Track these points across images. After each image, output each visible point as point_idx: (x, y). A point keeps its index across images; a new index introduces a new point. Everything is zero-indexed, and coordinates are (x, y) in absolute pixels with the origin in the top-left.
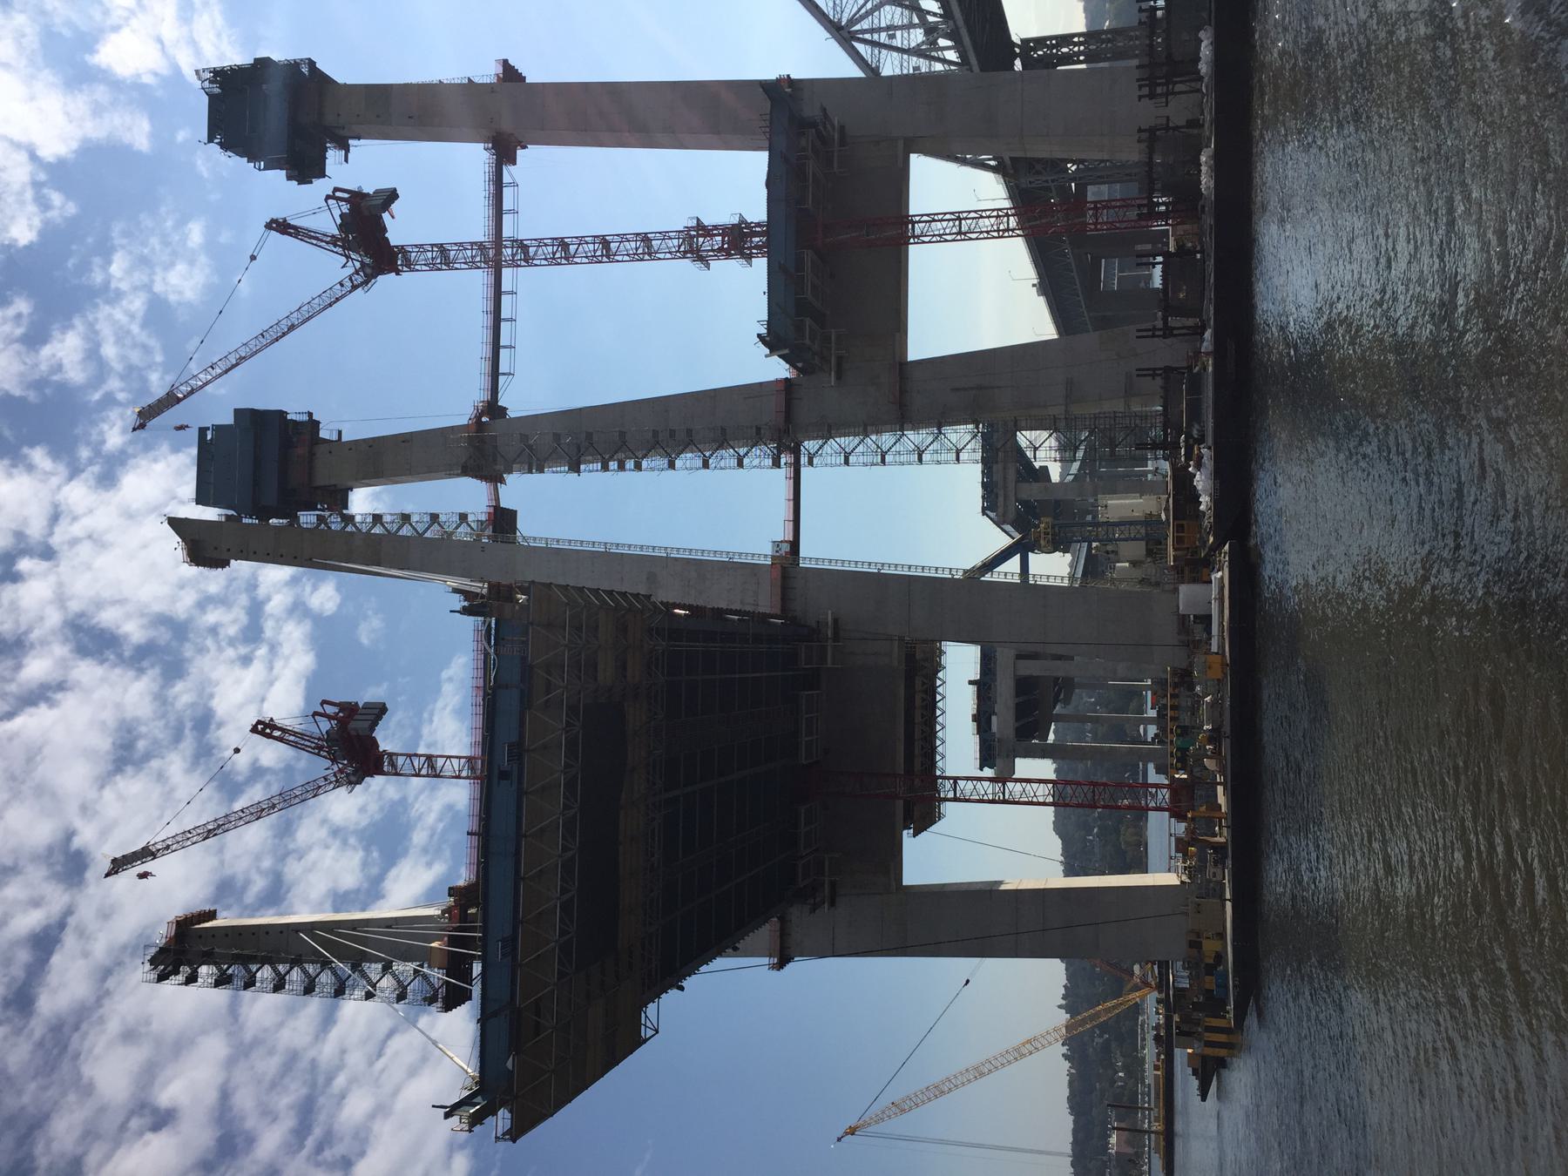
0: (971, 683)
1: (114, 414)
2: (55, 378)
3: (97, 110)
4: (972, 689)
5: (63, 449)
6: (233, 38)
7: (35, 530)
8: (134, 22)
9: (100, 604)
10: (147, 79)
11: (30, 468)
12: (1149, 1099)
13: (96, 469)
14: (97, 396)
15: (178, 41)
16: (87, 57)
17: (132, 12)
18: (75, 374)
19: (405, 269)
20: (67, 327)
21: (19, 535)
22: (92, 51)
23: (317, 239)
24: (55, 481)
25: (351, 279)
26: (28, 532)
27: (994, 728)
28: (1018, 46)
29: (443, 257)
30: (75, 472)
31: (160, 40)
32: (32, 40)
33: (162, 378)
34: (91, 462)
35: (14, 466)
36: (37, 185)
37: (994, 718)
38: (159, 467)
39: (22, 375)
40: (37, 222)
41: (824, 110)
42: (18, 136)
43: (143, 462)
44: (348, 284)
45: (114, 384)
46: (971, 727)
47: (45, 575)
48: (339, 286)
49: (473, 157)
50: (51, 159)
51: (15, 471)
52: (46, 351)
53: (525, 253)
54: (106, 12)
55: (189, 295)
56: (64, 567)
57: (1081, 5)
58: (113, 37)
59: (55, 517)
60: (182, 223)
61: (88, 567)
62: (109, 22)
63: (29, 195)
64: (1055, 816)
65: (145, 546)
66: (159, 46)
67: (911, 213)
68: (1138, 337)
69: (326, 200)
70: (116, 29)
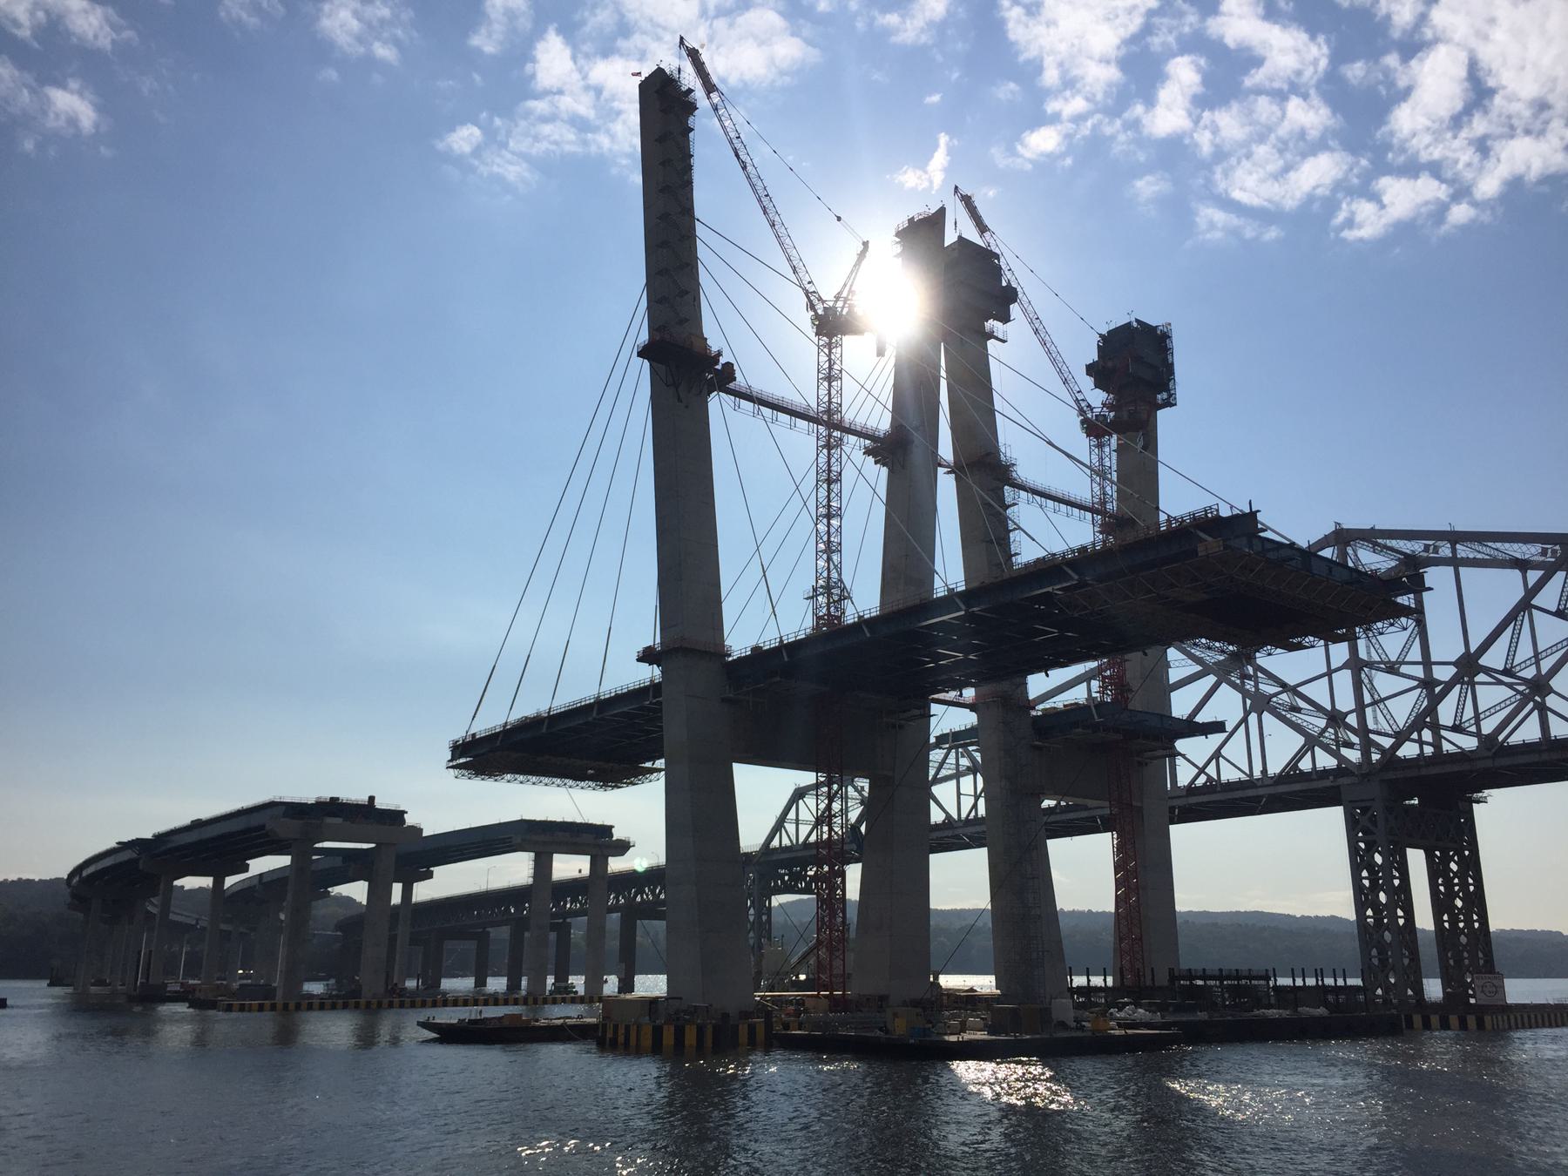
0: (372, 799)
4: (362, 798)
6: (552, 155)
8: (576, 76)
10: (529, 67)
12: (494, 1000)
15: (557, 107)
16: (555, 25)
22: (559, 32)
27: (329, 820)
31: (560, 92)
37: (339, 820)
46: (326, 794)
54: (587, 56)
55: (326, 23)
57: (1566, 933)
58: (568, 52)
60: (397, 43)
64: (1097, 913)
66: (555, 90)
68: (1316, 970)
70: (574, 58)
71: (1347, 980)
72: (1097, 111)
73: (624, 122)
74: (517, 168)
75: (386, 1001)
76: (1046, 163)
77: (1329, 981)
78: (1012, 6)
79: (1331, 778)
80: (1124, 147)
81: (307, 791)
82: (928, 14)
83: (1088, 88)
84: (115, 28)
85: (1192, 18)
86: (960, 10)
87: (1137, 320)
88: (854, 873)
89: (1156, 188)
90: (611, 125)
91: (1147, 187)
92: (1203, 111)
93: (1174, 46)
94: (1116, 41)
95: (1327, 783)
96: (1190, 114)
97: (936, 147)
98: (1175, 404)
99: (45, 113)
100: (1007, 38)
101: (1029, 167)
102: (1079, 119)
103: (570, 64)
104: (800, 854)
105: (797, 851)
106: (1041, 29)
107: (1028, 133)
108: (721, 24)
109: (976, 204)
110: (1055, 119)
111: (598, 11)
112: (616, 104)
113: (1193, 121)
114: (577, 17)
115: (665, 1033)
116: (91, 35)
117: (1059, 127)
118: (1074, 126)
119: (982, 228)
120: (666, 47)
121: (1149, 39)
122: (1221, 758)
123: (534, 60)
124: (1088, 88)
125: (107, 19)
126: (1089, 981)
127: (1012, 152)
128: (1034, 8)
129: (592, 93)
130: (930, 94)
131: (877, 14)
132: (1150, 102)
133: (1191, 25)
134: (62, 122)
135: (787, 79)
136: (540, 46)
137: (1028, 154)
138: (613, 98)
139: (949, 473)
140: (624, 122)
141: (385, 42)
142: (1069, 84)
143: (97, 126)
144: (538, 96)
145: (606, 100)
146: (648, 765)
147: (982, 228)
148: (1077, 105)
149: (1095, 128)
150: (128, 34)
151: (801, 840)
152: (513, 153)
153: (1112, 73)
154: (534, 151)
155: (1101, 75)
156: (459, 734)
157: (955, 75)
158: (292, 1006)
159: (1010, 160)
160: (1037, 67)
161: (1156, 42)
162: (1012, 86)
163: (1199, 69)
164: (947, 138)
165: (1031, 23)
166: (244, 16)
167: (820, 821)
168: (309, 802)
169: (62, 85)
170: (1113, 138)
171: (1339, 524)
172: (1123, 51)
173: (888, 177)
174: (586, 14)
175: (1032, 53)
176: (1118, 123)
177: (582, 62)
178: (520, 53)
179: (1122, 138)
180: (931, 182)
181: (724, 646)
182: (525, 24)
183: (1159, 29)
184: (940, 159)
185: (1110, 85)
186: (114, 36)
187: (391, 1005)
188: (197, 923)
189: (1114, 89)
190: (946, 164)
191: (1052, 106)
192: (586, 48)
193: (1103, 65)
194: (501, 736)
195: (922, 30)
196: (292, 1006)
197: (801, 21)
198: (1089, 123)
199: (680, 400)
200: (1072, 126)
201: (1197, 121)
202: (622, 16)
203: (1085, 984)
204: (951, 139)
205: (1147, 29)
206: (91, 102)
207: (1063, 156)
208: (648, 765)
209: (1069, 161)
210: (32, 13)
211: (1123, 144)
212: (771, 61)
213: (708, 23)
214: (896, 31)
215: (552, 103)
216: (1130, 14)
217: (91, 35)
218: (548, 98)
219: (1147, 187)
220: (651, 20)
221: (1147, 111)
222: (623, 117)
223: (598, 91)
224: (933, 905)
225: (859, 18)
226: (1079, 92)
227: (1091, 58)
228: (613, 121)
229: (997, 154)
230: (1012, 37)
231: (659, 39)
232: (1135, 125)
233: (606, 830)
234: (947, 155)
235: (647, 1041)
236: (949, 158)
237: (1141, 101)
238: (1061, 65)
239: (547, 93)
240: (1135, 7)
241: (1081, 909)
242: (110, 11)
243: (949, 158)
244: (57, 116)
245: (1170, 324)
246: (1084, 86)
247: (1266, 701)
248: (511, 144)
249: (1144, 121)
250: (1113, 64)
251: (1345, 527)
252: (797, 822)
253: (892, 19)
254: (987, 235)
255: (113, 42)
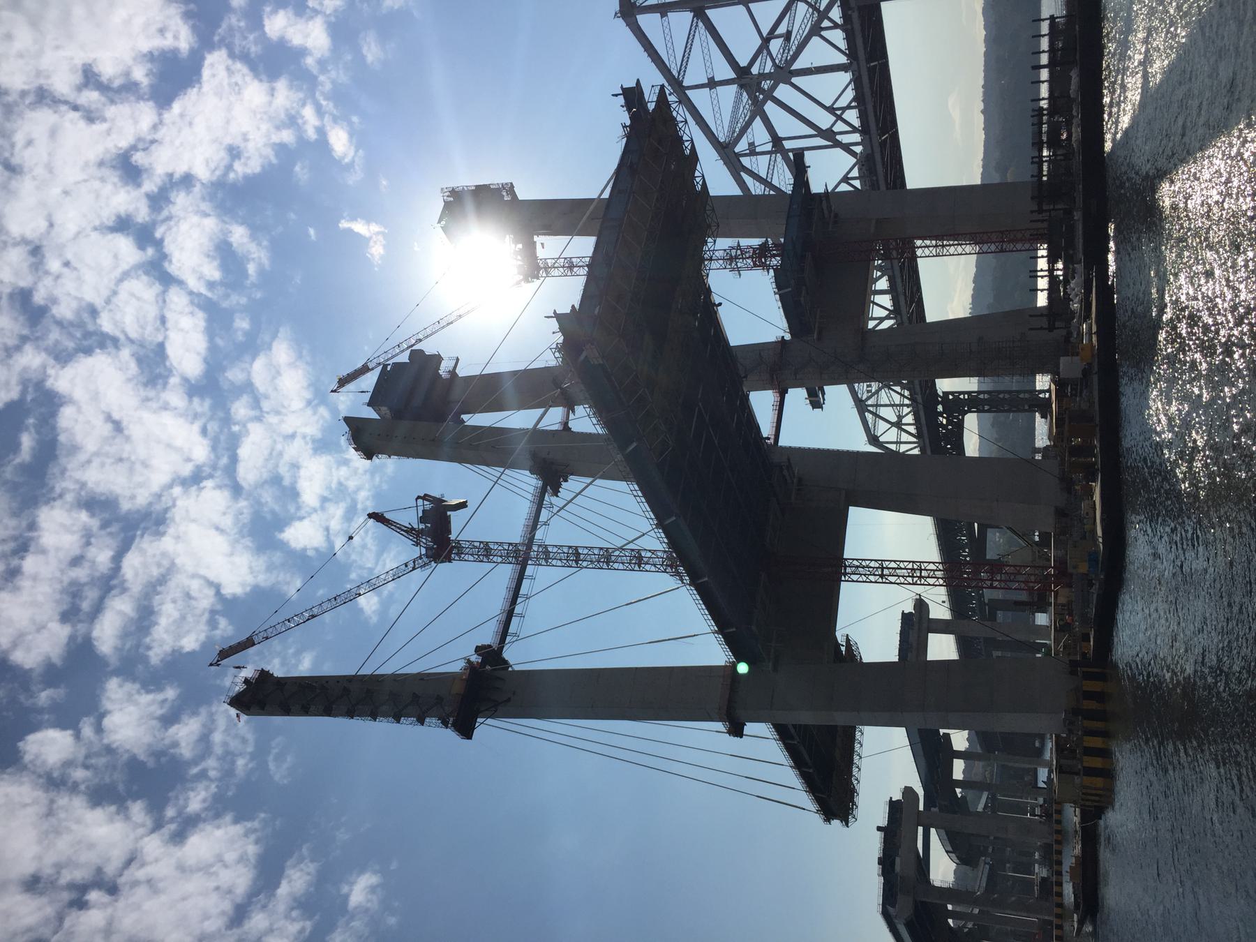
0: (879, 829)
1: (201, 786)
2: (172, 751)
3: (270, 568)
5: (156, 808)
7: (110, 870)
8: (314, 517)
9: (200, 88)
10: (310, 553)
11: (127, 818)
13: (173, 827)
14: (195, 771)
15: (339, 532)
16: (276, 533)
17: (315, 510)
18: (186, 752)
19: (457, 558)
20: (195, 713)
21: (99, 870)
22: (282, 531)
23: (399, 528)
24: (141, 831)
25: (414, 562)
26: (105, 870)
27: (898, 868)
28: (940, 397)
29: (485, 552)
30: (158, 826)
31: (327, 529)
32: (246, 518)
33: (246, 765)
34: (172, 820)
35: (118, 813)
36: (213, 612)
37: (898, 860)
38: (219, 833)
39: (149, 745)
40: (202, 637)
41: (789, 460)
42: (212, 576)
43: (209, 828)
44: (411, 565)
45: (211, 763)
46: (875, 869)
47: (104, 906)
48: (404, 566)
49: (527, 481)
50: (228, 597)
51: (118, 817)
52: (173, 730)
53: (546, 556)
54: (299, 508)
56: (121, 904)
58: (297, 524)
59: (129, 862)
60: (299, 653)
61: (138, 907)
62: (298, 514)
63: (206, 616)
65: (184, 899)
66: (326, 533)
67: (845, 557)
68: (1030, 277)
69: (416, 500)
70: (301, 519)
71: (1043, 33)
72: (313, 97)
73: (347, 479)
74: (388, 561)
75: (1056, 827)
76: (358, 138)
77: (1044, 59)
78: (234, 170)
79: (850, 12)
80: (341, 72)
81: (873, 884)
82: (245, 240)
83: (295, 105)
84: (301, 860)
85: (233, 20)
86: (240, 213)
87: (439, 222)
88: (945, 385)
89: (373, 45)
90: (350, 490)
91: (372, 51)
92: (308, 7)
93: (256, 34)
94: (256, 83)
95: (855, 15)
96: (311, 18)
97: (350, 231)
98: (511, 183)
99: (367, 910)
100: (259, 174)
101: (361, 152)
102: (320, 111)
103: (306, 522)
104: (927, 441)
105: (924, 443)
106: (251, 145)
107: (334, 154)
108: (266, 405)
109: (345, 374)
110: (321, 132)
111: (263, 500)
112: (334, 486)
113: (316, 15)
114: (269, 517)
115: (1091, 745)
116: (308, 878)
117: (328, 128)
118: (327, 116)
119: (365, 370)
120: (286, 448)
121: (253, 55)
122: (835, 106)
123: (305, 550)
124: (295, 105)
125: (294, 866)
126: (1042, 290)
127: (350, 166)
128: (234, 152)
129: (327, 505)
130: (308, 236)
131: (249, 282)
132: (302, 52)
133: (239, 20)
134: (374, 898)
135: (305, 352)
136: (293, 544)
137: (351, 153)
138: (329, 488)
139: (573, 412)
140: (347, 479)
141: (299, 661)
142: (292, 121)
143: (375, 872)
144: (331, 544)
145: (331, 493)
146: (843, 649)
147: (365, 370)
148: (308, 113)
149: (327, 99)
150: (305, 851)
151: (915, 440)
152: (377, 564)
153: (281, 85)
154: (374, 548)
155: (284, 95)
156: (818, 819)
157: (292, 216)
158: (1059, 911)
159: (357, 167)
160: (281, 148)
161: (254, 50)
162: (297, 168)
163: (275, 12)
164: (343, 221)
165: (246, 155)
166: (285, 766)
167: (898, 425)
168: (883, 881)
169: (346, 898)
170: (333, 82)
171: (616, 14)
172: (264, 77)
173: (376, 269)
174: (266, 509)
175: (269, 152)
176: (322, 78)
177: (302, 513)
178: (298, 559)
179: (333, 74)
180: (378, 233)
181: (726, 666)
182: (278, 557)
183: (244, 48)
184: (359, 227)
185: (291, 87)
186: (306, 861)
187: (1059, 822)
188: (988, 864)
189: (295, 83)
190: (363, 222)
191: (311, 134)
192: (292, 509)
193: (276, 94)
194: (817, 794)
195: (259, 244)
196: (1059, 911)
197: (259, 342)
198: (324, 103)
199: (509, 700)
200: (327, 118)
201: (316, 12)
202: (266, 482)
203: (1046, 293)
204: (344, 218)
205: (245, 57)
206: (358, 875)
207: (350, 123)
208: (843, 649)
209: (355, 119)
210: (294, 920)
211: (221, 431)
212: (291, 365)
213: (265, 415)
214: (260, 265)
215: (337, 535)
216: (233, 73)
217: (308, 878)
218: (332, 538)
219: (372, 51)
220: (267, 460)
221: (310, 54)
222: (342, 479)
223: (324, 500)
224: (977, 180)
225: (253, 296)
226: (298, 112)
227: (270, 103)
228: (346, 488)
229: (354, 178)
230: (258, 170)
231: (281, 454)
232: (322, 63)
233: (906, 617)
234: (356, 220)
235: (1099, 782)
236: (359, 220)
237: (303, 61)
238: (278, 128)
239: (328, 537)
240: (228, 69)
241: (981, 94)
242: (288, 863)
243: (359, 220)
244: (368, 901)
245: (442, 189)
246: (293, 108)
247: (779, 70)
248: (369, 565)
249: (319, 56)
250: (275, 84)
251: (618, 9)
252: (898, 443)
253: (251, 269)
254: (371, 365)
255: (312, 861)
